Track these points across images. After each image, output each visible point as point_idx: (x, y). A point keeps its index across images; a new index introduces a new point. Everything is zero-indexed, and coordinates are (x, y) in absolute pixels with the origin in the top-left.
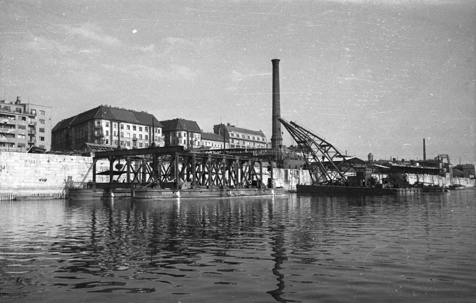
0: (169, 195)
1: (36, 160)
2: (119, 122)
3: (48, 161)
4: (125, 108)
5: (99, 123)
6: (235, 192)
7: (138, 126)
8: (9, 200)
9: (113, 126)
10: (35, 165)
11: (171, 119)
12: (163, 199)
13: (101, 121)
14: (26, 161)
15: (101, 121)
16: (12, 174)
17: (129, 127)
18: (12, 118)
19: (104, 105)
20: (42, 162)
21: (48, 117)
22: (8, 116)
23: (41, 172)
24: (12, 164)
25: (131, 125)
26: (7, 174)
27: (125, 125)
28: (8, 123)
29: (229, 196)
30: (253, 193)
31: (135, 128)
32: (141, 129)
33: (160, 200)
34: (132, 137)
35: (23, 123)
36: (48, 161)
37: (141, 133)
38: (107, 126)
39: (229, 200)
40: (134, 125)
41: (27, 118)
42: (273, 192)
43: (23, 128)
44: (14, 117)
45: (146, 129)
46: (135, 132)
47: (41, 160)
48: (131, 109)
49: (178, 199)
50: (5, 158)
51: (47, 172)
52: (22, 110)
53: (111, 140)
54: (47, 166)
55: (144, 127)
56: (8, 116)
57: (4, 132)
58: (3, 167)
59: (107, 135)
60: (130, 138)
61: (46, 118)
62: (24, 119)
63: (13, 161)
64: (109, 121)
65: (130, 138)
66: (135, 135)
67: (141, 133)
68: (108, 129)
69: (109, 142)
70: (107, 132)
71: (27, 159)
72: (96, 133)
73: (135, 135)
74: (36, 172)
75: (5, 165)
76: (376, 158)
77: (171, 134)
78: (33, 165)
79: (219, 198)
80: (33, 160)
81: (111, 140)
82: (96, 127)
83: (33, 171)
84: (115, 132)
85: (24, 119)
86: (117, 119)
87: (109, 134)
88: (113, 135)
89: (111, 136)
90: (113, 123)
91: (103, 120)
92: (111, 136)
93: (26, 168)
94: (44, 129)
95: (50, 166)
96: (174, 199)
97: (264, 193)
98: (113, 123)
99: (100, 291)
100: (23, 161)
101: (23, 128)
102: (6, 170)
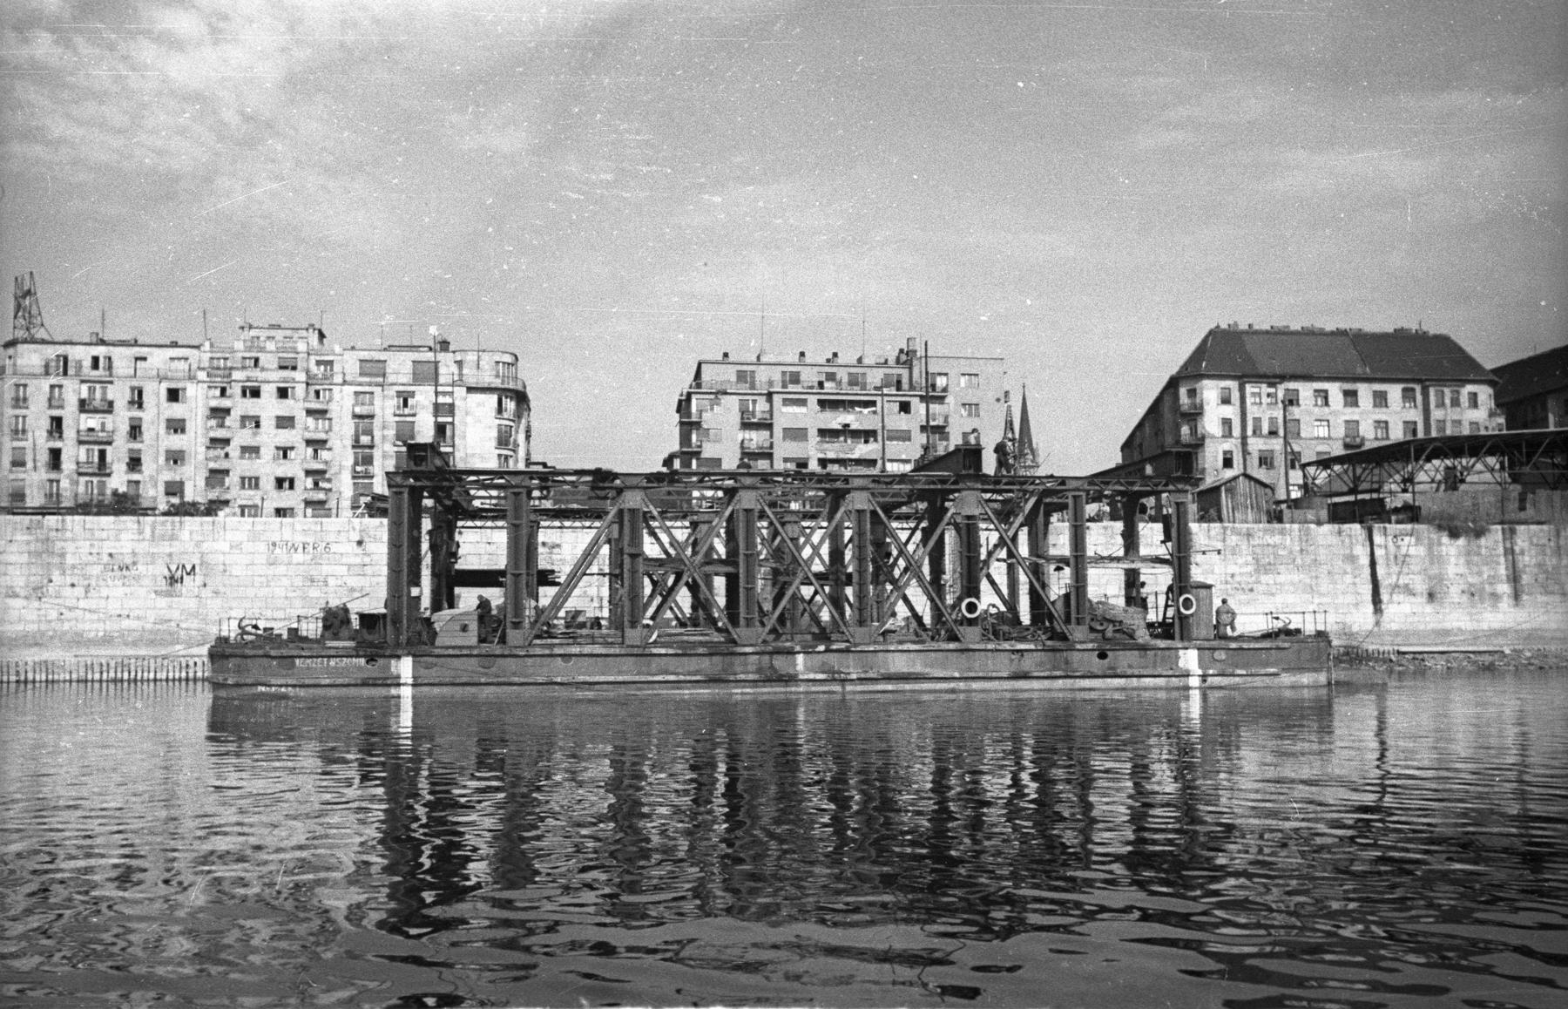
0: (336, 672)
1: (310, 540)
2: (1273, 379)
3: (360, 543)
4: (1318, 325)
5: (1192, 393)
6: (833, 659)
7: (1365, 391)
8: (135, 680)
9: (1249, 400)
10: (308, 557)
11: (1296, 326)
12: (302, 692)
13: (1198, 386)
14: (274, 544)
15: (1198, 386)
16: (222, 589)
17: (1324, 396)
18: (866, 411)
19: (1224, 326)
20: (334, 548)
21: (990, 394)
22: (853, 404)
23: (331, 581)
24: (221, 558)
25: (1335, 390)
26: (203, 591)
27: (1305, 390)
28: (854, 427)
29: (791, 679)
30: (1003, 665)
31: (1351, 397)
32: (1380, 399)
33: (285, 697)
34: (1340, 432)
35: (899, 422)
36: (360, 543)
37: (1381, 415)
38: (1226, 401)
39: (790, 705)
40: (1349, 386)
41: (915, 402)
42: (1189, 659)
43: (905, 436)
44: (873, 403)
45: (1408, 395)
46: (1352, 414)
47: (331, 538)
48: (1343, 326)
49: (406, 693)
50: (197, 537)
51: (353, 582)
52: (905, 380)
53: (1245, 453)
54: (358, 560)
55: (1394, 391)
56: (853, 404)
57: (842, 456)
58: (189, 568)
59: (1228, 434)
60: (1330, 438)
61: (986, 396)
62: (905, 407)
63: (225, 547)
64: (1233, 384)
65: (1330, 438)
66: (1352, 425)
67: (1381, 415)
68: (1231, 412)
69: (1237, 459)
70: (1227, 423)
71: (276, 537)
72: (1185, 430)
73: (1352, 425)
74: (312, 581)
75: (197, 562)
76: (1256, 327)
77: (1551, 403)
78: (299, 557)
79: (704, 692)
80: (299, 539)
81: (1245, 453)
82: (1185, 408)
83: (298, 582)
84: (1257, 420)
85: (905, 407)
86: (1262, 370)
87: (1236, 432)
88: (1249, 432)
89: (1244, 438)
90: (1249, 389)
91: (1206, 382)
92: (1244, 438)
93: (271, 571)
94: (278, 427)
95: (367, 560)
96: (382, 691)
97: (1096, 664)
98: (1249, 389)
99: (886, 957)
100: (262, 547)
101: (905, 436)
102: (199, 579)
